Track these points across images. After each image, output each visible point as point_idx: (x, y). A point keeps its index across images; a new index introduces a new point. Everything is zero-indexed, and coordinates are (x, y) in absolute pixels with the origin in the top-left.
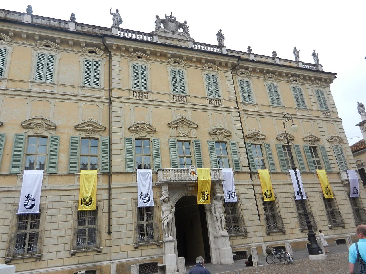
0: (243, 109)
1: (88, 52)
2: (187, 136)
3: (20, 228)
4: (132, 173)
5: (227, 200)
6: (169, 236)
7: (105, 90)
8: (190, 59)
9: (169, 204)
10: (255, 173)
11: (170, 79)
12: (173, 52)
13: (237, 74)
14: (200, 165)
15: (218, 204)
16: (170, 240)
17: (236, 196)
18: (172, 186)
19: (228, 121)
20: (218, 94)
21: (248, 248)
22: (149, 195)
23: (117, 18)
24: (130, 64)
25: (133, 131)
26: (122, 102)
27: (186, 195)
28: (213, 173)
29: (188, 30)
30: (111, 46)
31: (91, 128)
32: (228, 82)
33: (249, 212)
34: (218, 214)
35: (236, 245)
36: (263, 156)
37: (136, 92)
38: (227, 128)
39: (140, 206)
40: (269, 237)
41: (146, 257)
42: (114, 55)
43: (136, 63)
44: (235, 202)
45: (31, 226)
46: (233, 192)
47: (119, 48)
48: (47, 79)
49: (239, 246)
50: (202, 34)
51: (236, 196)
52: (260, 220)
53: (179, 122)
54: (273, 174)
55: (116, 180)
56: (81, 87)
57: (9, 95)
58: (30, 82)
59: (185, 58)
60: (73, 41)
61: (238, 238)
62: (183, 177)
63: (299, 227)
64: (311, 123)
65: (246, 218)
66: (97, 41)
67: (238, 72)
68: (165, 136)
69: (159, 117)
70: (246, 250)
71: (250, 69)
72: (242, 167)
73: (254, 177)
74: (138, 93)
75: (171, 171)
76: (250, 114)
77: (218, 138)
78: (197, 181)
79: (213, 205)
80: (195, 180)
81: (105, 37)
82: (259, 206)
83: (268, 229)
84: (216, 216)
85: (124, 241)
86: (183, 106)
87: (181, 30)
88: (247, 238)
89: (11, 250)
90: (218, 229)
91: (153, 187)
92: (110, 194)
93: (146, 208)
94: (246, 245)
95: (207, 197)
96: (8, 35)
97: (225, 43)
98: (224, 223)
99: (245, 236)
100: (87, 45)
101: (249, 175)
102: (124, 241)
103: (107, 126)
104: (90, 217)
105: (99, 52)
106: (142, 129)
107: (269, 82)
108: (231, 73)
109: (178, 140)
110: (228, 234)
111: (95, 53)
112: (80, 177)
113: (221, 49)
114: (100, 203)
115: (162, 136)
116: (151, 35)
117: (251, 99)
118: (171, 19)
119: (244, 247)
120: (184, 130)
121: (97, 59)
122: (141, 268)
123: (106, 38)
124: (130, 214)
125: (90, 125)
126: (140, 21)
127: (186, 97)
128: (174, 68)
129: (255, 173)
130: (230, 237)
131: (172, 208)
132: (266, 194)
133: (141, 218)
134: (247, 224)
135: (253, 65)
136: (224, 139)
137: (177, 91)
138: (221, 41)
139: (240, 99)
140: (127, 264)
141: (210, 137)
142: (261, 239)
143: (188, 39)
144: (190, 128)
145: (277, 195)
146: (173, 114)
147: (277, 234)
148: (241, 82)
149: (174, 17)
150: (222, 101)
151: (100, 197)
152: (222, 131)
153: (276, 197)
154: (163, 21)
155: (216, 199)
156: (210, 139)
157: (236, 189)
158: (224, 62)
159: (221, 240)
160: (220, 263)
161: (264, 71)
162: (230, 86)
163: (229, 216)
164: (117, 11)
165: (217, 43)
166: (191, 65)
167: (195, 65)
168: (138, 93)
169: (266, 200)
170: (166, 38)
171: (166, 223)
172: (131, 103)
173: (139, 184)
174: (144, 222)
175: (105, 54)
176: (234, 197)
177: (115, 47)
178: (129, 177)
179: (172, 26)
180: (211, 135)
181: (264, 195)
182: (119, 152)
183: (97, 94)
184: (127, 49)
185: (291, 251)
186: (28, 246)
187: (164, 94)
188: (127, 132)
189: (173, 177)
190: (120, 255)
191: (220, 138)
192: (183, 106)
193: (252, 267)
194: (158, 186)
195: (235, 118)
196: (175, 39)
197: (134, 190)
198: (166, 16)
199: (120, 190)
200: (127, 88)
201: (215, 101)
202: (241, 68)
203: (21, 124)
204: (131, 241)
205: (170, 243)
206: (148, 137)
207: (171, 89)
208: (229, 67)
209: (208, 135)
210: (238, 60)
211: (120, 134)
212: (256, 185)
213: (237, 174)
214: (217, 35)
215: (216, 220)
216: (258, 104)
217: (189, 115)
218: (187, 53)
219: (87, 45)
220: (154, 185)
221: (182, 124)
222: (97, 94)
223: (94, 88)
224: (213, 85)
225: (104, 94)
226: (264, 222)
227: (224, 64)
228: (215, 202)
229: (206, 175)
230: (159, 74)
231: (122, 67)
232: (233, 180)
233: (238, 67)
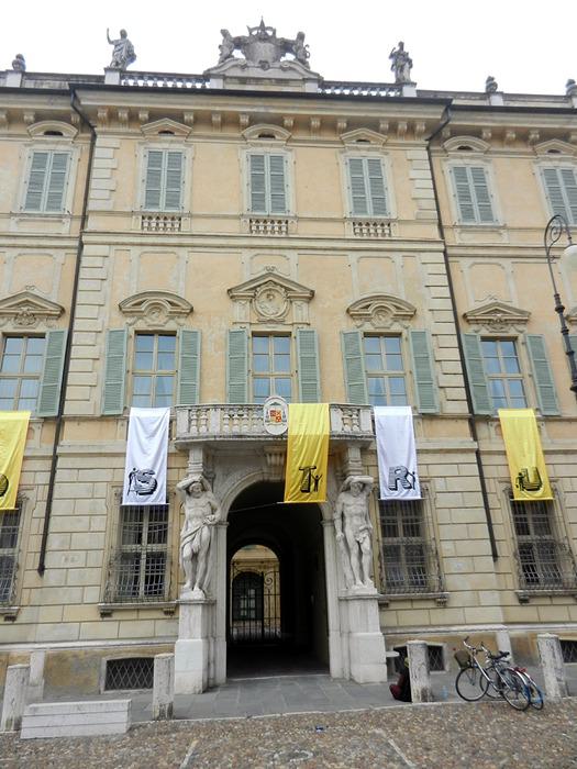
0: (458, 242)
1: (41, 133)
2: (282, 322)
3: (124, 539)
4: (116, 418)
5: (386, 495)
6: (196, 588)
7: (72, 217)
8: (302, 124)
9: (203, 500)
10: (487, 419)
11: (246, 178)
12: (255, 110)
13: (446, 151)
14: (310, 394)
15: (354, 505)
16: (192, 598)
17: (417, 482)
18: (218, 454)
19: (408, 275)
20: (380, 206)
21: (447, 638)
22: (154, 476)
23: (125, 52)
24: (142, 152)
25: (132, 312)
26: (109, 244)
27: (266, 478)
28: (338, 415)
29: (305, 55)
30: (95, 110)
31: (25, 309)
32: (413, 174)
33: (461, 532)
34: (349, 532)
35: (410, 627)
36: (520, 372)
37: (150, 218)
38: (403, 297)
39: (128, 504)
40: (525, 608)
41: (128, 642)
42: (104, 133)
43: (156, 146)
44: (414, 501)
45: (149, 537)
46: (408, 473)
47: (113, 116)
48: (49, 208)
49: (419, 630)
50: (346, 56)
51: (417, 482)
52: (495, 556)
53: (259, 286)
54: (550, 421)
55: (73, 436)
56: (15, 215)
57: (39, 247)
58: (11, 214)
59: (289, 122)
60: (6, 112)
61: (416, 605)
62: (247, 427)
63: (517, 586)
64: (503, 268)
65: (446, 548)
66: (61, 104)
67: (446, 144)
68: (217, 322)
69: (204, 279)
70: (440, 644)
71: (487, 134)
72: (444, 401)
73: (482, 430)
74: (162, 220)
75: (212, 411)
76: (483, 256)
77: (373, 325)
78: (286, 437)
79: (339, 508)
80: (282, 436)
81: (77, 92)
82: (497, 517)
83: (524, 586)
84: (345, 539)
85: (76, 594)
86: (274, 243)
87: (290, 57)
88: (445, 607)
89: (111, 589)
90: (349, 576)
91: (169, 455)
92: (53, 472)
93: (151, 512)
94: (442, 629)
95: (316, 484)
96: (283, 126)
97: (414, 75)
98: (366, 560)
99: (439, 602)
100: (39, 117)
101: (466, 426)
102: (76, 594)
103: (68, 306)
104: (405, 517)
105: (69, 130)
106: (156, 307)
107: (548, 165)
108: (428, 149)
109: (255, 334)
110: (375, 592)
111: (59, 134)
112: (499, 426)
113: (401, 90)
114: (29, 494)
115: (209, 323)
116: (206, 77)
117: (487, 214)
118: (263, 34)
119: (433, 635)
120: (273, 307)
121: (61, 148)
122: (115, 672)
123: (80, 94)
124: (99, 524)
125: (496, 311)
126: (181, 48)
127: (287, 222)
128: (259, 151)
129: (487, 419)
130: (383, 606)
131: (213, 511)
132: (521, 479)
133: (388, 529)
134: (450, 566)
135: (494, 121)
136: (391, 325)
137: (263, 209)
138: (402, 71)
139: (452, 213)
140: (75, 656)
141: (350, 320)
142: (498, 614)
143: (302, 75)
144: (290, 300)
145: (558, 485)
146: (244, 267)
147: (556, 601)
148: (460, 173)
149: (270, 28)
150: (392, 224)
151: (29, 479)
152: (162, 300)
153: (554, 491)
154: (239, 43)
155: (348, 489)
156: (349, 326)
157: (418, 464)
158: (403, 119)
159: (356, 606)
160: (347, 677)
161: (530, 134)
162: (418, 184)
163: (395, 539)
164: (123, 34)
165: (391, 78)
166: (307, 138)
167: (318, 138)
168: (162, 220)
169: (522, 496)
170: (243, 80)
171: (187, 552)
172: (133, 244)
173: (132, 448)
174: (399, 539)
175: (83, 135)
176: (410, 488)
177: (102, 114)
178: (109, 427)
179: (264, 50)
180: (352, 316)
181: (515, 482)
182: (88, 365)
183: (52, 229)
184: (133, 117)
185: (555, 662)
186: (146, 583)
187: (226, 217)
188: (116, 314)
189: (216, 426)
190: (60, 632)
191: (381, 321)
192: (274, 243)
193: (406, 705)
194: (182, 450)
195: (431, 268)
196: (270, 79)
197: (116, 462)
198: (251, 30)
199: (79, 462)
200: (128, 209)
201: (372, 228)
202: (456, 132)
203: (120, 309)
204: (94, 595)
205: (192, 608)
206: (396, 328)
207: (247, 203)
208: (420, 135)
209: (343, 316)
210: (446, 110)
211: (97, 320)
212: (490, 453)
213: (427, 422)
214: (392, 56)
215: (345, 552)
216: (509, 225)
217: (290, 266)
218: (293, 108)
219: (39, 117)
220: (173, 450)
221: (270, 290)
222: (52, 229)
223: (47, 216)
224: (366, 186)
225: (69, 228)
226: (509, 562)
227: (124, 115)
228: (344, 498)
229: (316, 421)
230: (216, 172)
231: (120, 162)
232: (410, 439)
233: (446, 132)
